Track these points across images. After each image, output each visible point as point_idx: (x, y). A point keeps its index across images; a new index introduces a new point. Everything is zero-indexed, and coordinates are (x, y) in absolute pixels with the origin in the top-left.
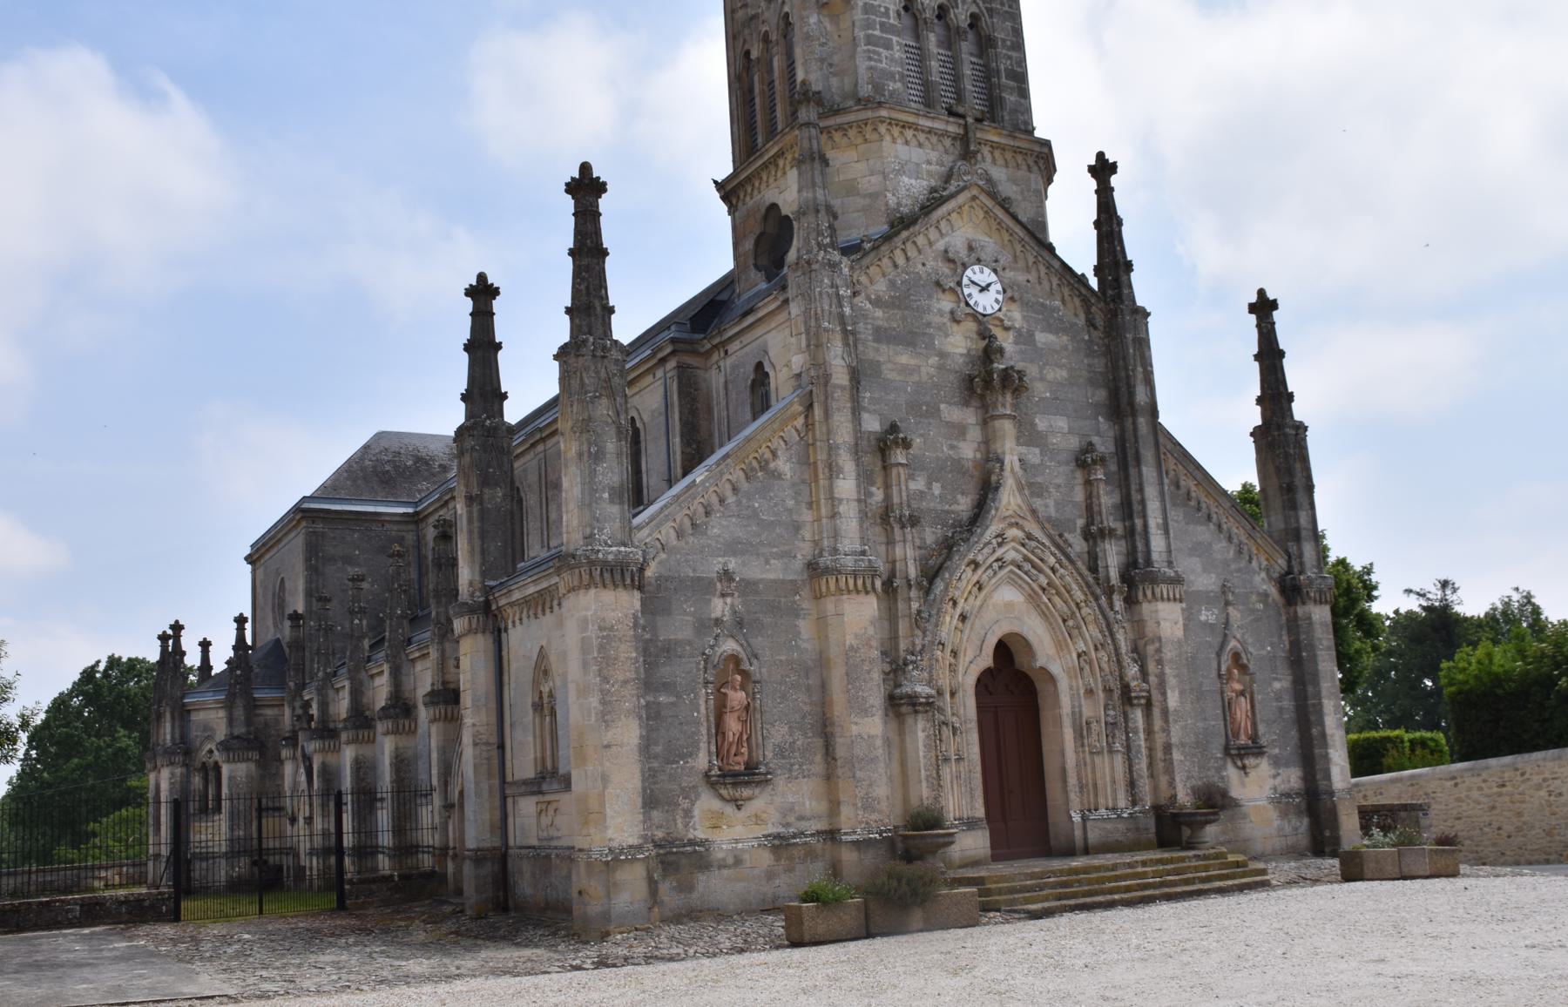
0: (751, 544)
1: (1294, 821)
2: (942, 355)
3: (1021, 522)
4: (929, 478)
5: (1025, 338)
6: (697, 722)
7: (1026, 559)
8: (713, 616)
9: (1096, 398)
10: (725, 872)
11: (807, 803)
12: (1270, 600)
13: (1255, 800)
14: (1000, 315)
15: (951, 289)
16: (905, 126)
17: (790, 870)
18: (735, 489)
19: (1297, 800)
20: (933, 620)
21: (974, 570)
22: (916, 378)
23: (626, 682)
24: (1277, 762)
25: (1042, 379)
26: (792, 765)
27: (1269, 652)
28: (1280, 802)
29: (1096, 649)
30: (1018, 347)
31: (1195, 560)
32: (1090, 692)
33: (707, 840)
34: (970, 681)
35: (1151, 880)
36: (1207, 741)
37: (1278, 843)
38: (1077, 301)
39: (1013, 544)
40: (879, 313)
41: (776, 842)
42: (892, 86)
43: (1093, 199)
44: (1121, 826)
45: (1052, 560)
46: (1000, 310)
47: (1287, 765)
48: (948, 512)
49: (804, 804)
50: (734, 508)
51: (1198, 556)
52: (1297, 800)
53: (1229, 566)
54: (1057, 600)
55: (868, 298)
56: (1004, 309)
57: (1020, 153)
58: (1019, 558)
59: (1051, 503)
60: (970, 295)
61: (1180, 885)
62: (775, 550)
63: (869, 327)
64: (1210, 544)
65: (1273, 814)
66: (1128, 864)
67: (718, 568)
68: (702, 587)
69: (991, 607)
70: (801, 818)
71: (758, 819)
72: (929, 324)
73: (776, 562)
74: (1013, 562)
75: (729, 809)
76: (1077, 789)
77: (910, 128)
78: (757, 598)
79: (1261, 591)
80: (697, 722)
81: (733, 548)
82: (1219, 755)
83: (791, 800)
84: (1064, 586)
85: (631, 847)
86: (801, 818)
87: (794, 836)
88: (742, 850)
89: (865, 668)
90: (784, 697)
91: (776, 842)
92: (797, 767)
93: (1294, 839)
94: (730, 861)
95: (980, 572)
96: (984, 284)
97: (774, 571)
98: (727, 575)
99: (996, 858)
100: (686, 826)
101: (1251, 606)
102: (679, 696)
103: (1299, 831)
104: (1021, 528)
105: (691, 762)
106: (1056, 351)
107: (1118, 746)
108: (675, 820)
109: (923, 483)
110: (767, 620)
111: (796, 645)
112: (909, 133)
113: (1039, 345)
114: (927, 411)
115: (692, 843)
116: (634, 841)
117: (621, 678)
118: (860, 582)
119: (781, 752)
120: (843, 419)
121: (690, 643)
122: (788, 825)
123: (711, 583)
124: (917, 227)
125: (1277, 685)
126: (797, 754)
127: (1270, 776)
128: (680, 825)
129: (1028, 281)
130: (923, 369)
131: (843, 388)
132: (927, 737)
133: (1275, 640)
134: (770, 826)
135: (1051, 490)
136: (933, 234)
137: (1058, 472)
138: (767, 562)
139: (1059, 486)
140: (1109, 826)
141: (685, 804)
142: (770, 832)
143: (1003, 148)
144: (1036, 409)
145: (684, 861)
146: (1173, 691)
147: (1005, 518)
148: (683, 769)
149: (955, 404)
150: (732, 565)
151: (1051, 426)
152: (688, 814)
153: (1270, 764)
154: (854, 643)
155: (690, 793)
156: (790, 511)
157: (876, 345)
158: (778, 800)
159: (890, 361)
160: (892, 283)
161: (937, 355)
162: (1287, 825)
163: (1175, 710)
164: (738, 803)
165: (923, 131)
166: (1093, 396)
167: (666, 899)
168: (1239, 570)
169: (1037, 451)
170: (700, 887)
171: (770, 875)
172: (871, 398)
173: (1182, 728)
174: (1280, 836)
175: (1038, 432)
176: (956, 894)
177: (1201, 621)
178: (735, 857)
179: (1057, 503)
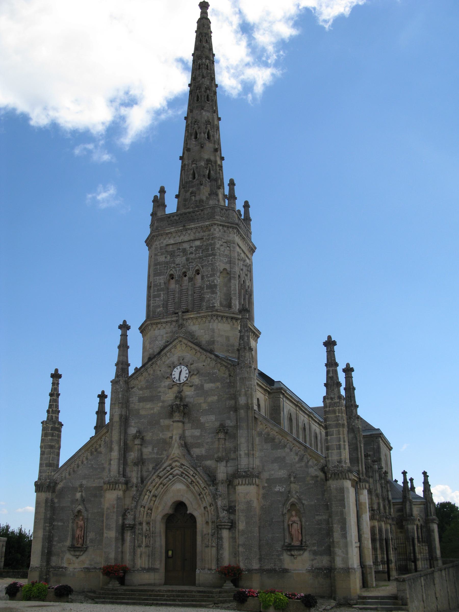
2: (163, 402)
3: (179, 459)
5: (199, 388)
7: (183, 473)
14: (187, 382)
16: (157, 324)
21: (160, 479)
28: (313, 572)
29: (210, 506)
30: (195, 392)
32: (207, 523)
33: (66, 567)
34: (159, 517)
38: (224, 368)
40: (141, 392)
43: (119, 338)
45: (192, 473)
46: (187, 380)
54: (196, 487)
56: (189, 379)
57: (204, 317)
58: (180, 473)
60: (186, 377)
68: (74, 490)
72: (160, 392)
73: (97, 480)
74: (177, 474)
75: (74, 558)
77: (159, 324)
82: (279, 549)
83: (93, 557)
84: (198, 482)
85: (36, 567)
92: (96, 546)
97: (96, 483)
98: (81, 486)
99: (166, 584)
105: (65, 544)
107: (214, 544)
112: (159, 326)
113: (205, 389)
116: (38, 565)
118: (111, 486)
128: (60, 562)
129: (204, 366)
139: (208, 442)
142: (86, 567)
143: (196, 318)
152: (62, 559)
156: (103, 464)
161: (161, 402)
164: (78, 557)
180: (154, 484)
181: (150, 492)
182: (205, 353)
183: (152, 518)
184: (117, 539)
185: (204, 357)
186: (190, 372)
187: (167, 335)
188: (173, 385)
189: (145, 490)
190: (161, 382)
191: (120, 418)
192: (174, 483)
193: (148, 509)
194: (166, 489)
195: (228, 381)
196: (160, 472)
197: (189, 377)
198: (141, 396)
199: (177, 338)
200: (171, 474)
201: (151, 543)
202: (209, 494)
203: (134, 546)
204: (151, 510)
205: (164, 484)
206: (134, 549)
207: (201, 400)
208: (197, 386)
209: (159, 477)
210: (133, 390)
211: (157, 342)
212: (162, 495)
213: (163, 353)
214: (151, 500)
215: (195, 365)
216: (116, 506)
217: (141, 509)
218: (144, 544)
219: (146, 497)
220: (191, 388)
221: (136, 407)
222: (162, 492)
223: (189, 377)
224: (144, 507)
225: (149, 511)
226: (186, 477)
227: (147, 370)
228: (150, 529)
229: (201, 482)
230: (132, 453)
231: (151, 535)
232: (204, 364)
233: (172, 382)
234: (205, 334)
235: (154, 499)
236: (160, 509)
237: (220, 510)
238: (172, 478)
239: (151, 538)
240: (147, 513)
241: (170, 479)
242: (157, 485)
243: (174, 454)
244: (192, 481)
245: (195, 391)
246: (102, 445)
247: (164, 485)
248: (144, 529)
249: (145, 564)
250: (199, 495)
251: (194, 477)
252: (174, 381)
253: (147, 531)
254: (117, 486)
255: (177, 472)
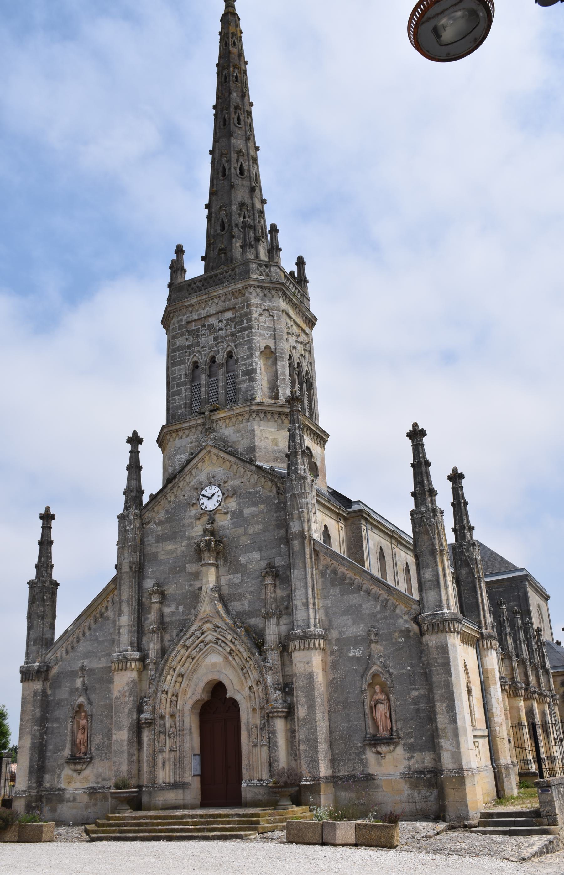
0: (93, 652)
1: (424, 792)
2: (189, 539)
3: (211, 619)
4: (177, 604)
6: (66, 735)
8: (76, 687)
9: (280, 535)
10: (69, 804)
11: (107, 772)
12: (412, 634)
13: (389, 775)
14: (220, 508)
15: (194, 504)
16: (177, 431)
17: (95, 805)
18: (90, 629)
19: (429, 776)
20: (157, 680)
21: (187, 650)
22: (175, 555)
23: (28, 720)
24: (411, 749)
25: (246, 534)
26: (102, 754)
27: (409, 670)
31: (347, 617)
33: (65, 789)
34: (188, 707)
35: (190, 827)
36: (350, 736)
37: (408, 807)
38: (269, 483)
39: (209, 632)
40: (159, 528)
41: (91, 791)
42: (180, 412)
44: (262, 791)
45: (229, 637)
46: (220, 505)
47: (421, 750)
48: (186, 620)
49: (106, 773)
50: (88, 637)
51: (350, 615)
52: (429, 776)
53: (375, 616)
54: (236, 658)
55: (155, 523)
56: (222, 504)
59: (246, 602)
61: (194, 832)
62: (103, 653)
63: (154, 536)
64: (360, 605)
65: (405, 789)
66: (191, 816)
67: (80, 665)
68: (73, 674)
69: (203, 667)
70: (104, 780)
71: (86, 779)
74: (211, 642)
75: (75, 775)
76: (248, 767)
77: (180, 431)
78: (95, 677)
79: (403, 629)
80: (66, 735)
81: (87, 655)
86: (104, 780)
87: (100, 788)
88: (77, 794)
89: (122, 706)
90: (101, 722)
91: (91, 791)
92: (104, 755)
93: (424, 805)
94: (71, 799)
95: (189, 650)
96: (210, 495)
100: (58, 782)
101: (393, 640)
102: (60, 724)
103: (429, 799)
104: (211, 622)
106: (256, 516)
108: (54, 779)
109: (174, 607)
110: (97, 686)
111: (109, 697)
112: (180, 433)
113: (245, 516)
114: (179, 570)
115: (59, 789)
117: (27, 718)
118: (120, 665)
119: (98, 748)
120: (125, 588)
121: (67, 699)
122: (98, 783)
123: (77, 672)
124: (177, 480)
125: (415, 693)
126: (105, 749)
127: (405, 759)
129: (242, 483)
130: (179, 549)
131: (127, 573)
132: (149, 740)
133: (415, 661)
134: (91, 783)
135: (247, 595)
136: (188, 479)
137: (252, 584)
138: (100, 659)
139: (252, 592)
140: (256, 791)
141: (58, 771)
143: (230, 418)
144: (241, 552)
145: (54, 798)
146: (303, 706)
147: (202, 619)
148: (59, 756)
149: (194, 562)
150: (86, 662)
151: (250, 559)
152: (59, 776)
153: (405, 750)
154: (118, 695)
155: (61, 767)
157: (156, 544)
158: (95, 770)
159: (162, 550)
160: (167, 511)
161: (186, 540)
162: (416, 794)
163: (304, 718)
164: (79, 772)
165: (187, 429)
166: (278, 534)
167: (46, 815)
168: (385, 618)
169: (239, 575)
170: (59, 811)
171: (87, 807)
172: (152, 571)
173: (308, 729)
174: (409, 802)
175: (241, 565)
176: (34, 825)
177: (349, 657)
178: (74, 797)
179: (249, 602)
180: (178, 658)
181: (174, 670)
182: (242, 464)
183: (178, 707)
184: (130, 742)
185: (242, 470)
186: (223, 494)
187: (191, 445)
188: (201, 515)
189: (167, 668)
190: (186, 511)
191: (131, 568)
192: (207, 655)
193: (173, 695)
194: (196, 664)
195: (276, 501)
196: (187, 640)
197: (223, 501)
198: (159, 533)
199: (205, 447)
200: (202, 642)
201: (178, 746)
202: (255, 667)
203: (154, 751)
204: (177, 696)
205: (193, 656)
206: (154, 754)
207: (241, 530)
208: (234, 512)
209: (186, 648)
210: (150, 526)
211: (178, 456)
212: (191, 674)
213: (186, 469)
214: (176, 681)
215: (230, 483)
216: (127, 694)
217: (163, 695)
218: (168, 746)
219: (169, 677)
220: (225, 516)
221: (154, 550)
222: (191, 669)
223: (223, 501)
224: (167, 693)
225: (174, 698)
226: (223, 644)
227: (165, 496)
228: (175, 725)
229: (242, 650)
230: (149, 616)
231: (178, 733)
232: (243, 480)
233: (200, 510)
234: (243, 439)
235: (180, 679)
236: (189, 694)
237: (271, 690)
238: (204, 646)
239: (178, 737)
240: (171, 701)
241: (201, 650)
242: (183, 659)
243: (205, 611)
244: (231, 650)
245: (231, 519)
246: (109, 608)
247: (193, 659)
248: (168, 725)
249: (169, 778)
250: (242, 669)
251: (233, 643)
252: (202, 509)
253: (171, 727)
254: (129, 664)
255: (210, 638)
